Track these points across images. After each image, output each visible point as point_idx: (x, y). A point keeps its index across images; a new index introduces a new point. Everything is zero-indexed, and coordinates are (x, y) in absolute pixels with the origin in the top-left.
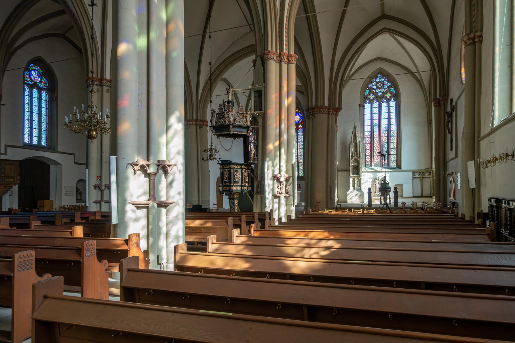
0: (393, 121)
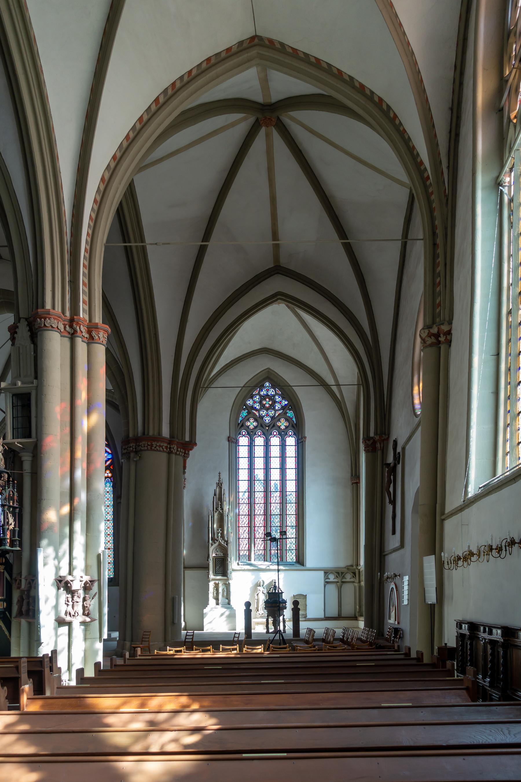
0: (291, 474)
